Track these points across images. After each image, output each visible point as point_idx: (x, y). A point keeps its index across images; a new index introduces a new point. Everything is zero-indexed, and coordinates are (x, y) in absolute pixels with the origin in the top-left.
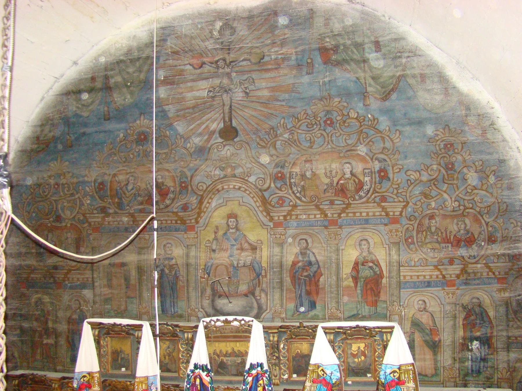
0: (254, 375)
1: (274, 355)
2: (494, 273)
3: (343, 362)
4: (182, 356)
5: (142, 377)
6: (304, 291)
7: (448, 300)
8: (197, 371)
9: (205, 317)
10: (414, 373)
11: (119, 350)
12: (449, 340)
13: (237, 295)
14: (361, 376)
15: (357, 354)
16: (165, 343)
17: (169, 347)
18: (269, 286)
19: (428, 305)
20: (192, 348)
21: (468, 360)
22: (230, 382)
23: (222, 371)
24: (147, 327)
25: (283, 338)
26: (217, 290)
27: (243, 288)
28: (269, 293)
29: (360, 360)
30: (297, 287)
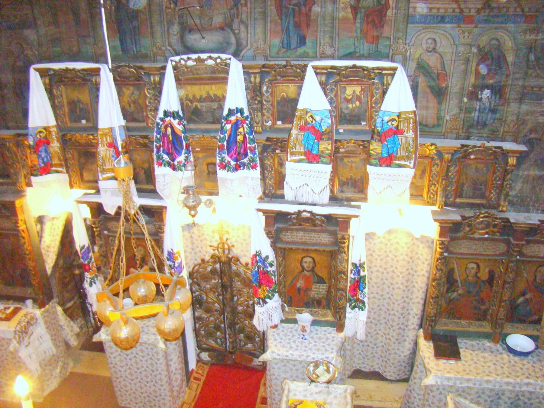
2: (522, 10)
3: (336, 107)
4: (150, 103)
5: (106, 129)
6: (292, 22)
7: (462, 41)
8: (168, 119)
10: (415, 122)
11: (76, 99)
12: (458, 87)
13: (210, 29)
15: (352, 99)
16: (128, 89)
17: (133, 94)
18: (249, 17)
20: (160, 92)
21: (476, 110)
22: (207, 131)
24: (105, 71)
26: (187, 23)
27: (218, 20)
29: (354, 105)
30: (284, 18)
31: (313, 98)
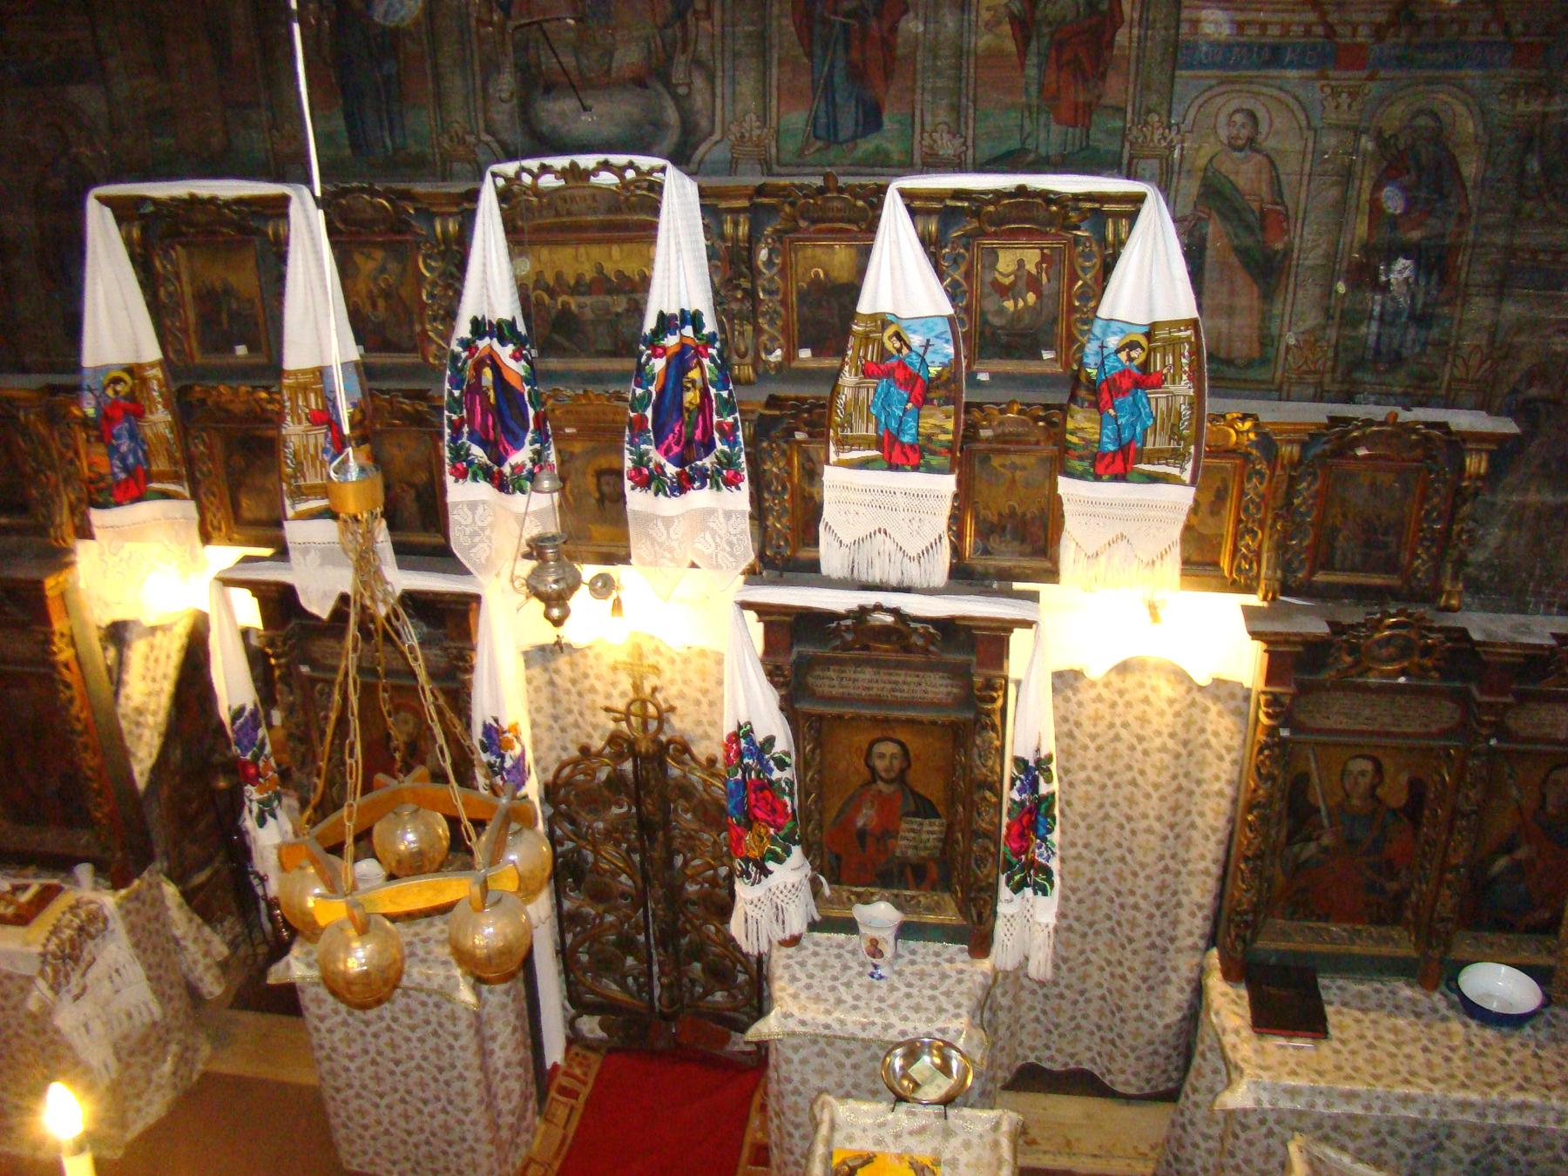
0: (670, 352)
1: (738, 287)
2: (1506, 28)
3: (967, 309)
4: (431, 296)
5: (304, 372)
6: (840, 64)
7: (1332, 117)
8: (483, 344)
9: (498, 162)
10: (1196, 351)
11: (218, 285)
12: (1320, 251)
13: (605, 83)
14: (1020, 358)
15: (1013, 284)
16: (369, 257)
17: (383, 270)
19: (1264, 128)
20: (462, 266)
21: (1371, 317)
22: (598, 378)
23: (566, 344)
24: (303, 203)
25: (769, 229)
26: (539, 66)
27: (629, 57)
28: (719, 74)
29: (1021, 304)
31: (901, 281)
